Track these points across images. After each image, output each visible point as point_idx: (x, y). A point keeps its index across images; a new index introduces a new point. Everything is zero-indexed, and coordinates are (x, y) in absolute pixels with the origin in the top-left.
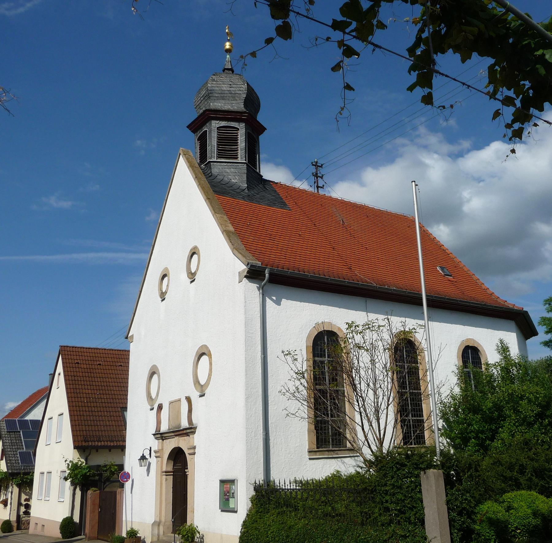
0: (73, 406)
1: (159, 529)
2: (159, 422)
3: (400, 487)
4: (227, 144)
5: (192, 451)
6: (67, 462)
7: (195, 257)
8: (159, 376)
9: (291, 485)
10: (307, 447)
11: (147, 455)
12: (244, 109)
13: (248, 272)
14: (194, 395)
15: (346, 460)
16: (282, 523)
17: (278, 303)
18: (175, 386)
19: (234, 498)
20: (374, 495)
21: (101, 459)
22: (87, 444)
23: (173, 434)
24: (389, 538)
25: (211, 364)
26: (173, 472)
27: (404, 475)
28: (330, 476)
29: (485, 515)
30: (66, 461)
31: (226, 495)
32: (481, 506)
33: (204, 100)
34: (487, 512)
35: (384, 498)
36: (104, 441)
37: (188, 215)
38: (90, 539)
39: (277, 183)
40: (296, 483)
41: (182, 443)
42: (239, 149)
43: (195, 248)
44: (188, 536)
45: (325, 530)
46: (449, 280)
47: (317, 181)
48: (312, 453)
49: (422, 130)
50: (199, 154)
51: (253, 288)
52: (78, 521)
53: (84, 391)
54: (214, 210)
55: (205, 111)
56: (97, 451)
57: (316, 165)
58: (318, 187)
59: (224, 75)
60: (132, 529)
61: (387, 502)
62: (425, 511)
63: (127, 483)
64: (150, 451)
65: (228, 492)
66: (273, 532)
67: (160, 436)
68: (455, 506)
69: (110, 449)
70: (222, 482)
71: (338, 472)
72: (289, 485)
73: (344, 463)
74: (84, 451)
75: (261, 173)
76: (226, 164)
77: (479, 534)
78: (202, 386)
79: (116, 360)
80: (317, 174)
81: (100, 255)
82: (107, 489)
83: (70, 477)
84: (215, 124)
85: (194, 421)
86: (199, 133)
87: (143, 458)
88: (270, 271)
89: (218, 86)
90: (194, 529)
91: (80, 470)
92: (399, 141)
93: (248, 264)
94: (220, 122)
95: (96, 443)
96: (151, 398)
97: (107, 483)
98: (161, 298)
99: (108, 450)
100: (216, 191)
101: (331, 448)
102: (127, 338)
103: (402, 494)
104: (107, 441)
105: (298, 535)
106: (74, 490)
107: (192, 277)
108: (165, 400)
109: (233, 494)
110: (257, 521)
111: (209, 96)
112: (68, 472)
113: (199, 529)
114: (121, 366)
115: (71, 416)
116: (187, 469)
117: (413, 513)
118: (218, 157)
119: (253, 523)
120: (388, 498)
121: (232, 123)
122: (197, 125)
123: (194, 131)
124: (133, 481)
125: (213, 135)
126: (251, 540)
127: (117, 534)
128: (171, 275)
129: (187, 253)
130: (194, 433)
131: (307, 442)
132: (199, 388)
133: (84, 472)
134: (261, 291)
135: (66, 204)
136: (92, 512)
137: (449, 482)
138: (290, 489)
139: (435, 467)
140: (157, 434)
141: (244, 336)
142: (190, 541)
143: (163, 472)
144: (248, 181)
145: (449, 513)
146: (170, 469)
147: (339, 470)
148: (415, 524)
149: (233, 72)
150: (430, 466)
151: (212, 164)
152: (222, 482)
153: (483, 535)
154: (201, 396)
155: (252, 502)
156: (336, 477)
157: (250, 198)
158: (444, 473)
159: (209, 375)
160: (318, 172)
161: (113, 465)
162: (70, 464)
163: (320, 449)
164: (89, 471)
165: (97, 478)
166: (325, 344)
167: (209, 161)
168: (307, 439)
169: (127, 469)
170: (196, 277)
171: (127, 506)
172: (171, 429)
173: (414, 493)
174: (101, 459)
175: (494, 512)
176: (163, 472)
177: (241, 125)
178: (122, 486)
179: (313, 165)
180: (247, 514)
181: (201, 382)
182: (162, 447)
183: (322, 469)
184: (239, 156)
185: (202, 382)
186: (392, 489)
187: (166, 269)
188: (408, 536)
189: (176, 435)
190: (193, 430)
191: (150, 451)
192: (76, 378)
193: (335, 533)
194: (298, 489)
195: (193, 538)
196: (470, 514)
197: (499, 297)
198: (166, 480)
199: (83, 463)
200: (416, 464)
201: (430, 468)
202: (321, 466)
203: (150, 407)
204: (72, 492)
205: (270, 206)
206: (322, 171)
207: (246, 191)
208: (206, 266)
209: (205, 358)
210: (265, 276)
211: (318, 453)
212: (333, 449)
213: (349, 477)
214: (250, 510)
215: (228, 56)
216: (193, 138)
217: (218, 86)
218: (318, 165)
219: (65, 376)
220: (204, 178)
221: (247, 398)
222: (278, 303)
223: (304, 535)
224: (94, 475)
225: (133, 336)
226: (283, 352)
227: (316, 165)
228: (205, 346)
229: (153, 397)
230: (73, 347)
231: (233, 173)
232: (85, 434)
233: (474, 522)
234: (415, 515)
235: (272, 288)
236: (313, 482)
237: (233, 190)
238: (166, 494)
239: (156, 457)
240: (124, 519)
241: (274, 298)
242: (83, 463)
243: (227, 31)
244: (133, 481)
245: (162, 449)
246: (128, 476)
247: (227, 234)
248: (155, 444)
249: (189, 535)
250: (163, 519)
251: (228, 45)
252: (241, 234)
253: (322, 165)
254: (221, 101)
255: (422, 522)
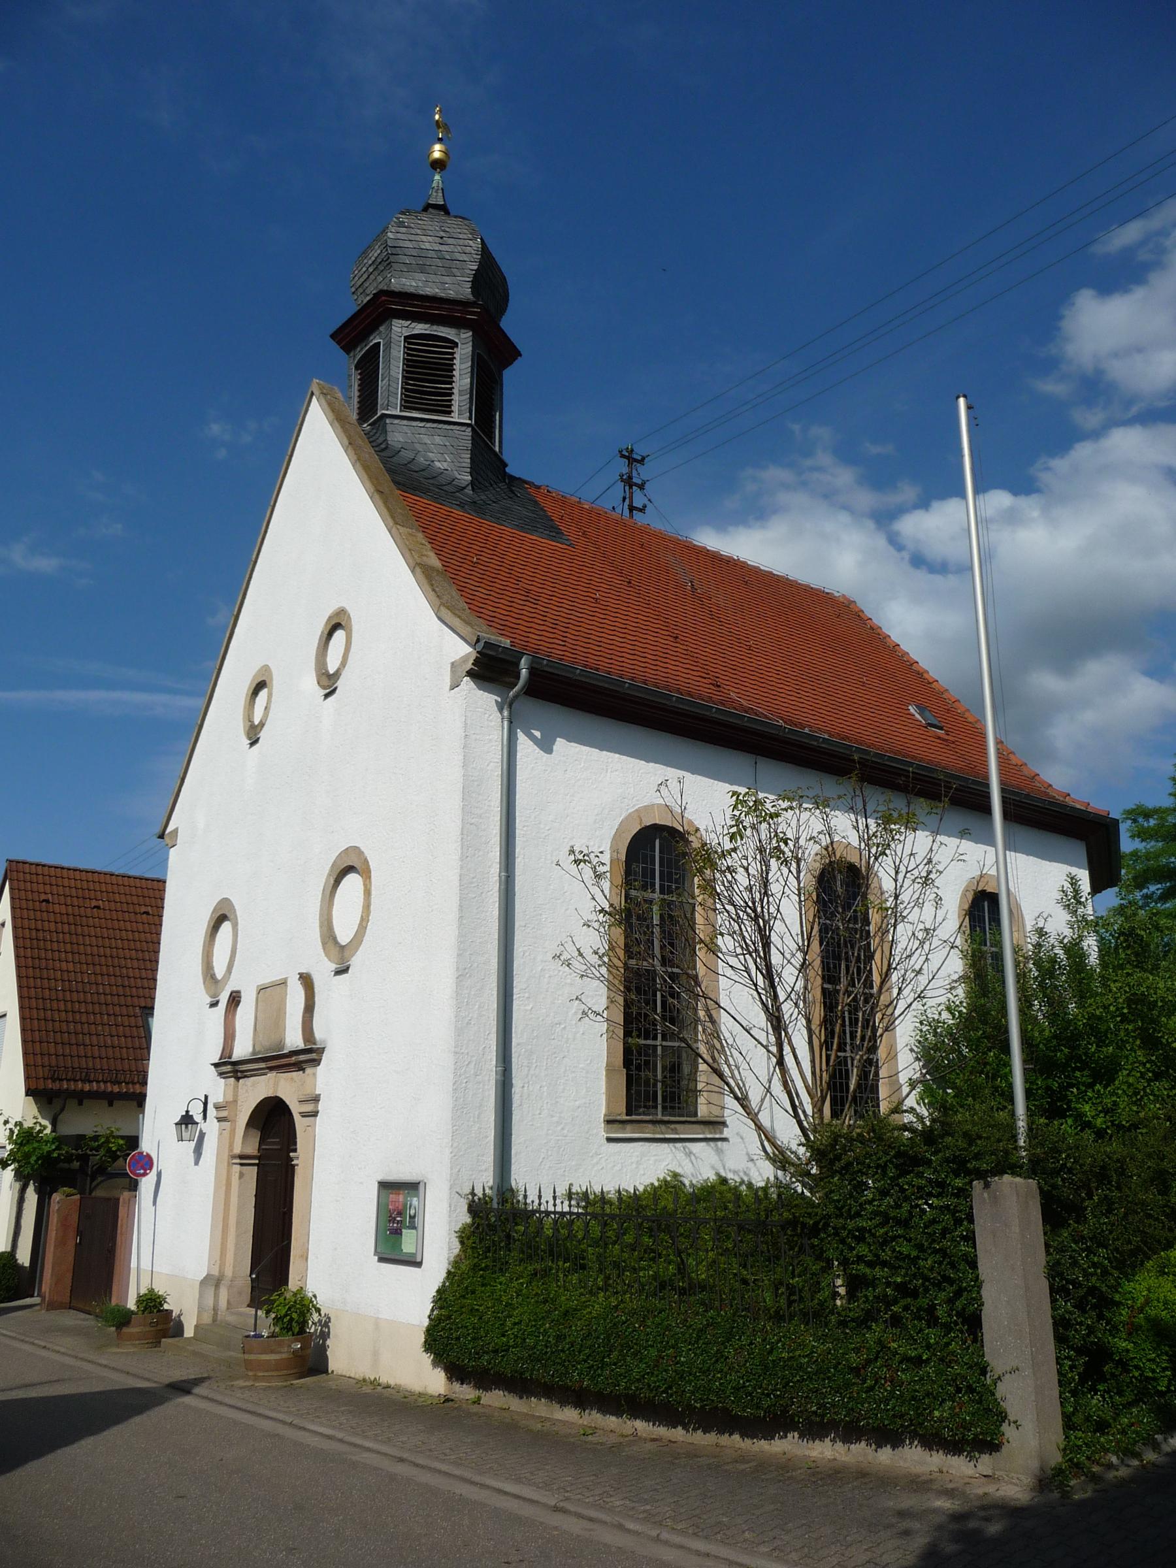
0: (30, 998)
1: (216, 1296)
2: (229, 1036)
3: (905, 1223)
4: (427, 382)
5: (308, 1108)
6: (8, 1126)
7: (340, 635)
8: (270, 696)
9: (558, 1201)
10: (603, 1111)
11: (196, 1112)
12: (471, 297)
13: (476, 662)
14: (322, 968)
15: (696, 1147)
16: (545, 1301)
17: (546, 746)
18: (274, 946)
19: (415, 1228)
20: (822, 1240)
21: (85, 1123)
22: (56, 1086)
23: (263, 1065)
24: (868, 1362)
25: (368, 893)
26: (259, 1158)
27: (920, 1188)
28: (656, 1184)
29: (1141, 1310)
30: (6, 1122)
31: (393, 1220)
32: (1128, 1286)
33: (376, 273)
34: (1148, 1301)
35: (852, 1249)
36: (98, 1082)
37: (329, 535)
38: (52, 1306)
39: (539, 487)
40: (570, 1199)
41: (285, 1086)
42: (455, 391)
43: (342, 612)
44: (292, 1319)
45: (668, 1328)
46: (939, 738)
47: (631, 494)
48: (615, 1126)
49: (824, 458)
50: (356, 400)
51: (483, 706)
52: (27, 1264)
53: (57, 964)
54: (393, 517)
55: (377, 296)
56: (80, 1103)
57: (630, 458)
58: (632, 508)
59: (424, 216)
60: (151, 1291)
61: (860, 1259)
62: (984, 1293)
63: (144, 1179)
64: (205, 1104)
65: (400, 1214)
66: (520, 1323)
67: (231, 1068)
68: (1068, 1282)
69: (111, 1099)
70: (386, 1186)
71: (676, 1175)
72: (551, 1202)
73: (689, 1154)
74: (50, 1102)
75: (505, 457)
76: (422, 424)
77: (1123, 1365)
78: (342, 948)
79: (140, 927)
80: (630, 478)
81: (116, 695)
82: (99, 1193)
83: (14, 1161)
84: (400, 329)
85: (318, 1035)
86: (360, 353)
87: (187, 1120)
88: (533, 662)
89: (412, 237)
90: (306, 1303)
91: (36, 1145)
92: (775, 474)
93: (478, 641)
94: (414, 324)
95: (80, 1085)
96: (213, 977)
97: (100, 1179)
98: (250, 739)
99: (105, 1103)
100: (400, 484)
101: (659, 1117)
102: (162, 836)
103: (909, 1240)
104: (105, 1082)
105: (590, 1334)
106: (23, 1191)
107: (329, 683)
108: (246, 982)
109: (412, 1217)
110: (473, 1292)
111: (386, 263)
112: (9, 1147)
113: (321, 1301)
114: (147, 913)
115: (23, 1019)
116: (295, 1150)
117: (942, 1295)
118: (405, 407)
119: (463, 1297)
120: (863, 1249)
121: (442, 328)
122: (355, 333)
123: (348, 348)
124: (159, 1175)
125: (394, 353)
126: (458, 1339)
127: (114, 1302)
128: (277, 683)
129: (319, 626)
130: (316, 1062)
131: (604, 1097)
132: (334, 951)
133: (46, 1148)
134: (506, 713)
135: (45, 564)
136: (61, 1243)
137: (1056, 1213)
138: (555, 1213)
139: (1014, 1169)
140: (225, 1064)
141: (459, 823)
142: (296, 1330)
143: (234, 1157)
144: (474, 469)
145: (1053, 1301)
146: (252, 1148)
147: (679, 1170)
148: (948, 1328)
149: (447, 213)
150: (1006, 1166)
151: (388, 421)
152: (386, 1186)
153: (1137, 1367)
154: (338, 972)
155: (462, 1243)
156: (671, 1186)
157: (478, 508)
158: (1040, 1188)
159: (362, 919)
160: (634, 474)
161: (114, 1137)
162: (16, 1132)
163: (634, 1117)
164: (58, 1148)
165: (76, 1165)
166: (657, 861)
167: (384, 416)
168: (604, 1090)
169: (147, 1145)
170: (340, 684)
171: (142, 1236)
172: (259, 1053)
173: (953, 1240)
174: (85, 1123)
175: (1166, 1303)
176: (234, 1157)
177: (463, 336)
178: (134, 1186)
179: (623, 456)
180: (449, 1273)
181: (339, 939)
182: (236, 1094)
183: (637, 1166)
184: (455, 408)
185: (344, 937)
186: (882, 1225)
187: (266, 669)
188: (928, 1361)
189: (271, 1069)
190: (314, 1056)
191: (205, 1104)
192: (41, 934)
193: (699, 1338)
194: (578, 1214)
195: (303, 1324)
196: (1103, 1303)
197: (1050, 785)
198: (241, 1175)
199: (45, 1127)
200: (955, 1159)
201: (1001, 1172)
202: (634, 1159)
203: (209, 1000)
204: (16, 1195)
205: (522, 529)
206: (642, 473)
207: (469, 491)
208: (367, 659)
209: (352, 882)
210: (518, 678)
211: (629, 1127)
212: (666, 1118)
213: (703, 1189)
214: (456, 1263)
215: (437, 177)
216: (347, 364)
217: (412, 237)
218: (635, 456)
219: (15, 928)
220: (368, 449)
221: (460, 978)
222: (546, 746)
223: (608, 1338)
224: (69, 1158)
225: (176, 831)
226: (572, 852)
227: (630, 458)
228: (356, 850)
229: (219, 976)
230: (38, 865)
231: (442, 448)
232: (54, 1063)
233: (1114, 1330)
234: (951, 1301)
235: (531, 707)
236: (620, 1199)
237: (440, 487)
238: (240, 1208)
239: (220, 1120)
240: (133, 1264)
241: (537, 734)
242: (45, 1127)
243: (437, 117)
244: (159, 1175)
245: (235, 1101)
246: (147, 1163)
247: (426, 574)
248: (218, 1089)
249: (295, 1316)
250: (229, 1272)
251: (437, 152)
252: (457, 572)
253: (643, 459)
254: (418, 275)
255: (973, 1323)
